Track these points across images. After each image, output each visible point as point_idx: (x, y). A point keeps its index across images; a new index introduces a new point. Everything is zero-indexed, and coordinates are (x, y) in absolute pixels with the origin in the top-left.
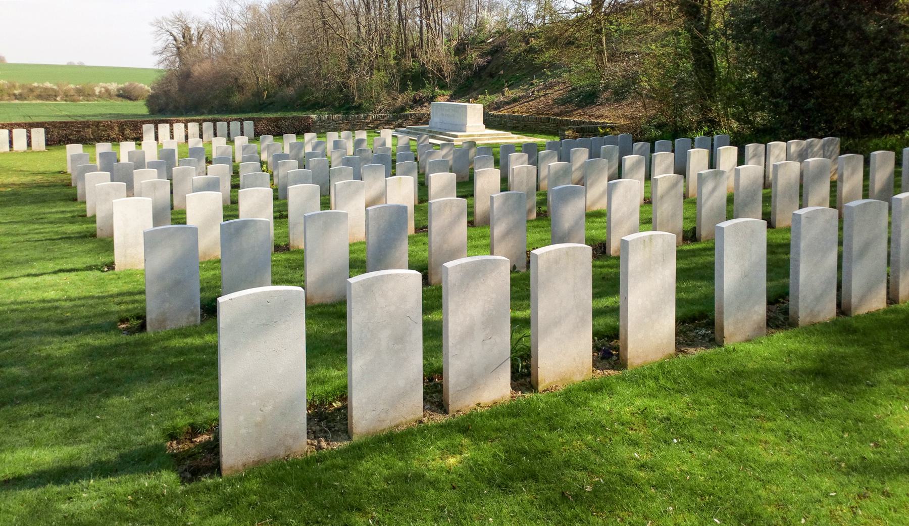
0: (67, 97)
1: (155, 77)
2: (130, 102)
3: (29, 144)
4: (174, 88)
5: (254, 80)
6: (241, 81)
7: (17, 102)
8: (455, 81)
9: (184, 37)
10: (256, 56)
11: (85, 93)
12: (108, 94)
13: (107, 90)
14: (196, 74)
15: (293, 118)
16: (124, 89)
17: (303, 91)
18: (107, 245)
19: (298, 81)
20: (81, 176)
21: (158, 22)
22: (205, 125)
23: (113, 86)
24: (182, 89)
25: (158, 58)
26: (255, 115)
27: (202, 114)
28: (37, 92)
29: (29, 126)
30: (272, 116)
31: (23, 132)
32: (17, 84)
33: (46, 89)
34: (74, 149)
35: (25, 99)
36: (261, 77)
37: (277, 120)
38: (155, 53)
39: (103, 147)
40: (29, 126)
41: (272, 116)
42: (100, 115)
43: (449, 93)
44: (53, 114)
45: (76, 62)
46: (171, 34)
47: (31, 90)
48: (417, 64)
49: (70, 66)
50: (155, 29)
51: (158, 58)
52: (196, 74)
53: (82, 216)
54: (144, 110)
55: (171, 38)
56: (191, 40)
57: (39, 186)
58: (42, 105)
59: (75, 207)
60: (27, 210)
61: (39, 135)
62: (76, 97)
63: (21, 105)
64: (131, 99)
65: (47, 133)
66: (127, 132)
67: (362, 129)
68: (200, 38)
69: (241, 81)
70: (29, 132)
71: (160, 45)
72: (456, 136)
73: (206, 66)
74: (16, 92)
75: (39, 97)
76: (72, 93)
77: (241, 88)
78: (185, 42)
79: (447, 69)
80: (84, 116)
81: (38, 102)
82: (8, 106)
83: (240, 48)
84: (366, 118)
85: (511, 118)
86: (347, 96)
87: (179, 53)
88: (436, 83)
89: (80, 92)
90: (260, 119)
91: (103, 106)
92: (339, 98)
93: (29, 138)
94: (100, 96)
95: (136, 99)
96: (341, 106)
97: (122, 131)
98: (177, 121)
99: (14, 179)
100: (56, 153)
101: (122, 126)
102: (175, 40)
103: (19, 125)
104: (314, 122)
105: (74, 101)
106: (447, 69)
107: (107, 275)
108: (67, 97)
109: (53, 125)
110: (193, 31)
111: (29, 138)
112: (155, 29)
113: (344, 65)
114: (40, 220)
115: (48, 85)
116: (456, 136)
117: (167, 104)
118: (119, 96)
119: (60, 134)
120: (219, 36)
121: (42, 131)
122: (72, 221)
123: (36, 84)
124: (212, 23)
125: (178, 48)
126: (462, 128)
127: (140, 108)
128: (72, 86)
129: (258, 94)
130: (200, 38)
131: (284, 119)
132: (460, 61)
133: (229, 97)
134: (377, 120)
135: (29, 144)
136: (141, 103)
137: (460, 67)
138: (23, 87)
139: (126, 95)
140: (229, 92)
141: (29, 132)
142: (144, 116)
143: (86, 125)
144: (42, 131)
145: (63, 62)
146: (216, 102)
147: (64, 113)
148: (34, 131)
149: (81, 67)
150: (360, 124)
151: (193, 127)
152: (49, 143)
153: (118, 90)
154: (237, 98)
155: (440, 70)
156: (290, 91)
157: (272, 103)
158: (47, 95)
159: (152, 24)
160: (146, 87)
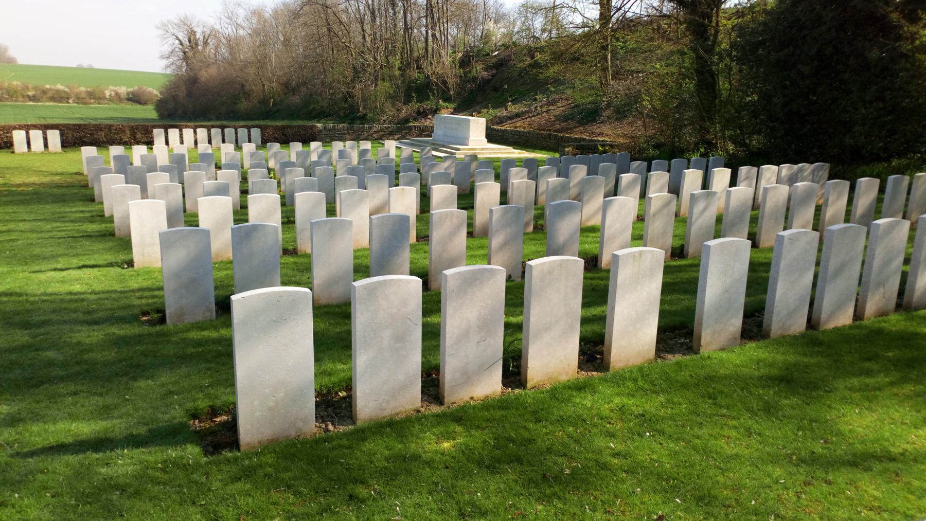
0: (79, 99)
1: (162, 81)
2: (139, 107)
3: (46, 145)
4: (182, 93)
5: (260, 87)
6: (247, 88)
7: (31, 103)
8: (459, 93)
9: (190, 41)
10: (261, 62)
11: (95, 96)
12: (117, 98)
13: (117, 94)
14: (203, 79)
15: (299, 126)
19: (303, 89)
21: (164, 25)
22: (213, 131)
23: (123, 90)
24: (190, 94)
25: (165, 62)
26: (262, 123)
27: (210, 120)
28: (50, 94)
30: (279, 123)
32: (30, 86)
33: (58, 91)
34: (89, 151)
35: (39, 101)
37: (283, 128)
38: (162, 57)
39: (116, 150)
42: (112, 118)
44: (67, 116)
45: (85, 65)
46: (177, 38)
47: (44, 92)
49: (80, 69)
50: (161, 32)
51: (165, 62)
52: (203, 79)
53: (101, 216)
54: (154, 115)
55: (177, 42)
56: (197, 44)
57: (58, 186)
58: (55, 107)
60: (50, 208)
61: (54, 137)
62: (87, 100)
63: (35, 106)
65: (62, 135)
66: (139, 136)
68: (206, 43)
70: (27, 133)
71: (167, 49)
72: (458, 149)
73: (213, 71)
75: (52, 99)
76: (83, 95)
77: (247, 95)
78: (191, 47)
79: (452, 82)
80: (96, 119)
81: (51, 104)
82: (24, 107)
84: (370, 128)
86: (352, 106)
87: (186, 58)
89: (91, 94)
90: (267, 127)
91: (115, 110)
97: (134, 135)
98: (186, 127)
100: (71, 155)
101: (134, 130)
102: (181, 44)
103: (35, 127)
104: (320, 131)
105: (85, 104)
106: (452, 82)
110: (199, 35)
112: (161, 32)
113: (349, 74)
115: (60, 87)
116: (458, 149)
118: (129, 99)
119: (75, 137)
120: (224, 41)
123: (48, 86)
124: (218, 27)
125: (185, 53)
127: (149, 112)
128: (83, 89)
129: (264, 101)
130: (206, 43)
131: (290, 127)
132: (465, 73)
134: (381, 130)
135: (46, 145)
136: (150, 107)
138: (35, 88)
139: (136, 99)
142: (153, 120)
143: (98, 128)
145: (73, 64)
147: (77, 116)
149: (91, 69)
153: (128, 94)
154: (243, 105)
155: (445, 82)
156: (296, 99)
157: (278, 111)
158: (59, 97)
159: (157, 28)
160: (155, 91)
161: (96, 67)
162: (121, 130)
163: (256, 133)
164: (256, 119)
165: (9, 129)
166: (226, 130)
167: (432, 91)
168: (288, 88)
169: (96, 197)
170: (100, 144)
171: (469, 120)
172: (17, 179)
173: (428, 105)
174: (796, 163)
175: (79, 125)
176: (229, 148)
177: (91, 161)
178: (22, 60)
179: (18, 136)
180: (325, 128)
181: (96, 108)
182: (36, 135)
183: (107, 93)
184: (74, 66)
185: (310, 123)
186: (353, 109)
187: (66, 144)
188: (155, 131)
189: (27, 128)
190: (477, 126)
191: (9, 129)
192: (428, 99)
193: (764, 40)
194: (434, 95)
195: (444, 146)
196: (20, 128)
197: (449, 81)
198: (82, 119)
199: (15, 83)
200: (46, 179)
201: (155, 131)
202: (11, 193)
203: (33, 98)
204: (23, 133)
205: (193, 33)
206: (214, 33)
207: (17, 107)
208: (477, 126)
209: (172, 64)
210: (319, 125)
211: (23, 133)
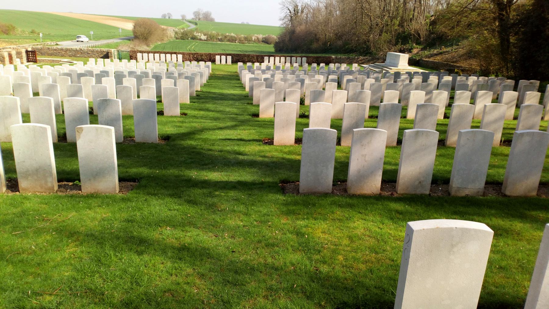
0: (241, 41)
2: (267, 45)
3: (226, 62)
4: (287, 39)
5: (324, 36)
6: (318, 36)
8: (426, 40)
9: (294, 11)
10: (326, 22)
11: (248, 40)
12: (258, 41)
13: (258, 38)
15: (324, 57)
16: (265, 38)
18: (245, 88)
21: (283, 2)
22: (287, 58)
23: (261, 36)
24: (290, 39)
25: (281, 22)
26: (308, 55)
27: (298, 53)
28: (228, 38)
31: (224, 57)
32: (220, 34)
33: (232, 36)
34: (240, 64)
35: (223, 41)
36: (327, 34)
38: (280, 20)
39: (249, 64)
40: (227, 55)
42: (254, 51)
43: (421, 47)
44: (234, 49)
45: (245, 22)
46: (289, 9)
47: (226, 37)
48: (401, 29)
49: (243, 25)
50: (281, 6)
53: (241, 83)
54: (273, 50)
55: (288, 11)
56: (298, 12)
57: (230, 76)
60: (227, 81)
61: (229, 58)
62: (244, 41)
63: (221, 44)
64: (268, 43)
65: (232, 58)
66: (259, 59)
68: (302, 12)
69: (318, 36)
70: (226, 57)
71: (283, 15)
72: (391, 69)
73: (303, 27)
75: (229, 41)
76: (243, 39)
77: (317, 40)
78: (295, 14)
79: (423, 33)
80: (246, 51)
81: (228, 43)
82: (216, 44)
83: (321, 18)
84: (358, 58)
85: (433, 63)
86: (368, 46)
87: (291, 20)
88: (415, 41)
89: (246, 39)
90: (310, 57)
91: (256, 47)
93: (226, 59)
94: (254, 41)
95: (270, 44)
97: (257, 59)
99: (222, 73)
100: (234, 66)
102: (290, 12)
103: (223, 54)
104: (333, 59)
105: (243, 43)
106: (423, 33)
108: (241, 41)
109: (234, 55)
110: (300, 8)
111: (226, 59)
112: (281, 6)
113: (367, 29)
115: (233, 34)
116: (391, 69)
118: (263, 41)
119: (237, 59)
120: (312, 11)
121: (181, 56)
122: (238, 84)
123: (227, 34)
124: (309, 3)
125: (291, 17)
126: (396, 65)
127: (271, 48)
128: (243, 36)
129: (325, 44)
130: (302, 12)
131: (320, 57)
132: (432, 29)
133: (311, 45)
134: (363, 59)
135: (226, 62)
136: (272, 45)
138: (222, 35)
139: (266, 41)
140: (311, 42)
141: (226, 57)
142: (272, 52)
143: (245, 55)
144: (181, 56)
145: (239, 22)
147: (239, 49)
148: (228, 57)
149: (248, 25)
151: (283, 59)
153: (263, 39)
154: (315, 46)
155: (419, 35)
156: (340, 43)
157: (331, 49)
158: (232, 40)
159: (280, 4)
160: (275, 37)
162: (253, 57)
166: (271, 58)
167: (410, 38)
168: (339, 36)
169: (254, 99)
170: (245, 62)
171: (400, 55)
172: (217, 73)
174: (529, 80)
175: (238, 54)
176: (288, 64)
177: (240, 67)
178: (217, 20)
179: (218, 58)
180: (336, 58)
181: (247, 46)
182: (223, 57)
184: (240, 23)
185: (330, 55)
186: (368, 48)
187: (234, 62)
188: (265, 58)
189: (221, 55)
190: (404, 58)
192: (408, 43)
193: (532, 21)
194: (412, 41)
195: (386, 68)
196: (218, 54)
198: (241, 51)
199: (213, 32)
200: (226, 73)
201: (265, 58)
202: (215, 77)
203: (221, 40)
204: (219, 56)
205: (297, 6)
206: (306, 6)
207: (214, 44)
208: (404, 58)
210: (333, 56)
211: (219, 56)
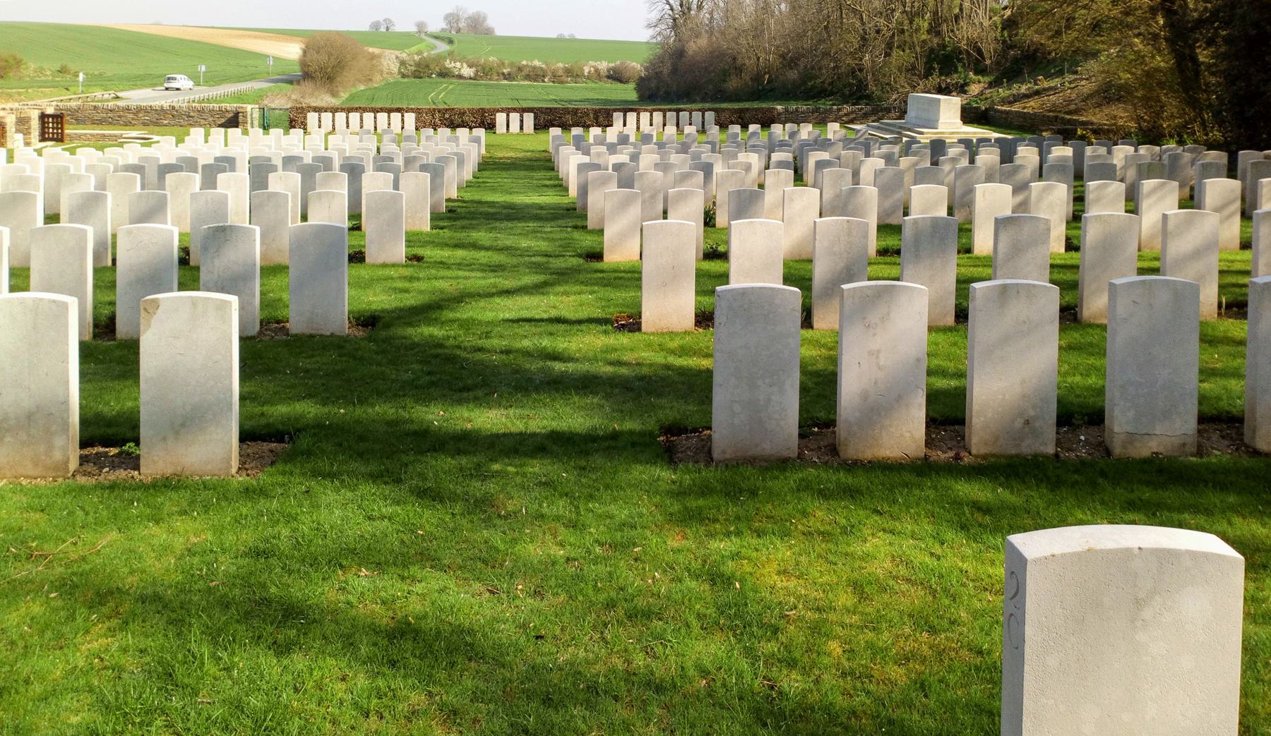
0: (556, 78)
1: (646, 55)
3: (521, 128)
6: (739, 62)
7: (506, 82)
8: (998, 63)
9: (681, 5)
10: (758, 30)
11: (573, 74)
12: (597, 75)
13: (597, 70)
14: (690, 53)
16: (614, 69)
17: (807, 76)
19: (802, 63)
20: (557, 150)
22: (668, 114)
23: (603, 66)
24: (674, 70)
25: (651, 32)
26: (717, 106)
27: (694, 102)
28: (526, 72)
29: (523, 111)
30: (736, 106)
31: (343, 115)
33: (535, 68)
34: (555, 131)
35: (514, 79)
36: (762, 56)
37: (742, 111)
38: (649, 26)
39: (576, 131)
40: (523, 111)
41: (736, 106)
42: (587, 100)
43: (987, 79)
45: (566, 35)
47: (520, 69)
49: (560, 40)
51: (651, 32)
52: (690, 53)
53: (557, 178)
54: (633, 96)
56: (689, 9)
58: (530, 86)
59: (552, 174)
61: (529, 119)
64: (621, 82)
65: (535, 118)
66: (601, 119)
67: (835, 121)
69: (739, 62)
70: (522, 116)
71: (655, 16)
73: (703, 42)
74: (505, 71)
75: (528, 77)
76: (560, 73)
77: (739, 70)
79: (989, 48)
80: (570, 101)
81: (526, 83)
82: (498, 87)
84: (839, 110)
86: (860, 81)
87: (675, 26)
88: (972, 66)
89: (568, 72)
90: (723, 110)
92: (851, 85)
93: (522, 121)
95: (627, 82)
96: (851, 95)
97: (596, 118)
98: (645, 110)
99: (512, 154)
100: (542, 136)
101: (596, 112)
102: (672, 9)
103: (515, 110)
104: (779, 114)
105: (562, 82)
106: (989, 48)
107: (624, 339)
108: (556, 78)
109: (540, 109)
111: (522, 121)
113: (855, 42)
114: (532, 178)
115: (537, 63)
117: (658, 88)
118: (608, 77)
119: (546, 119)
123: (524, 62)
125: (674, 20)
126: (932, 124)
127: (629, 92)
128: (560, 65)
129: (757, 78)
131: (747, 109)
132: (1010, 37)
135: (521, 128)
136: (632, 86)
137: (1007, 46)
138: (512, 65)
139: (616, 76)
140: (725, 75)
141: (522, 116)
143: (566, 111)
146: (711, 87)
148: (525, 115)
149: (573, 40)
150: (832, 116)
152: (538, 127)
154: (733, 83)
155: (979, 51)
156: (793, 75)
157: (772, 90)
158: (535, 75)
160: (637, 66)
161: (580, 36)
163: (710, 116)
164: (748, 100)
165: (494, 112)
167: (960, 60)
168: (790, 61)
173: (955, 79)
175: (551, 109)
176: (671, 130)
178: (500, 31)
179: (501, 118)
180: (786, 110)
181: (572, 88)
182: (515, 117)
183: (586, 70)
186: (862, 85)
188: (615, 114)
191: (494, 112)
192: (956, 71)
196: (502, 110)
197: (984, 47)
199: (491, 59)
200: (521, 155)
202: (495, 163)
203: (508, 77)
204: (504, 115)
207: (491, 86)
209: (660, 34)
210: (779, 107)
211: (504, 115)
